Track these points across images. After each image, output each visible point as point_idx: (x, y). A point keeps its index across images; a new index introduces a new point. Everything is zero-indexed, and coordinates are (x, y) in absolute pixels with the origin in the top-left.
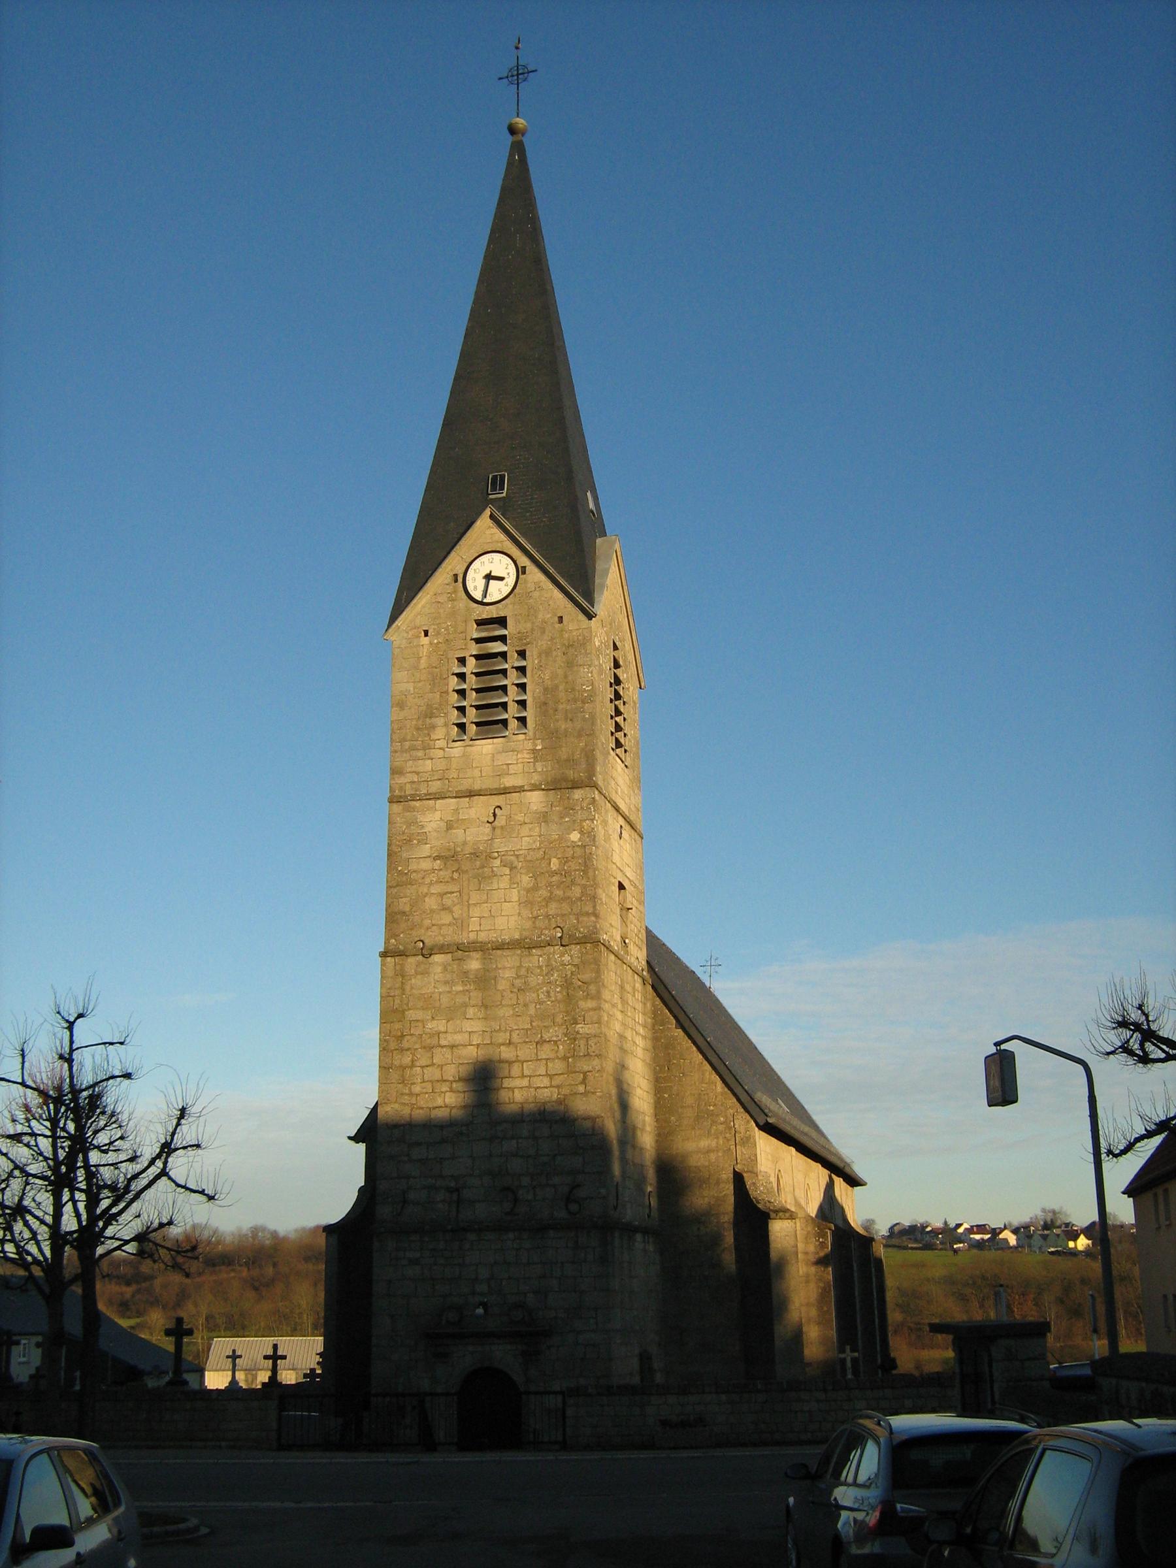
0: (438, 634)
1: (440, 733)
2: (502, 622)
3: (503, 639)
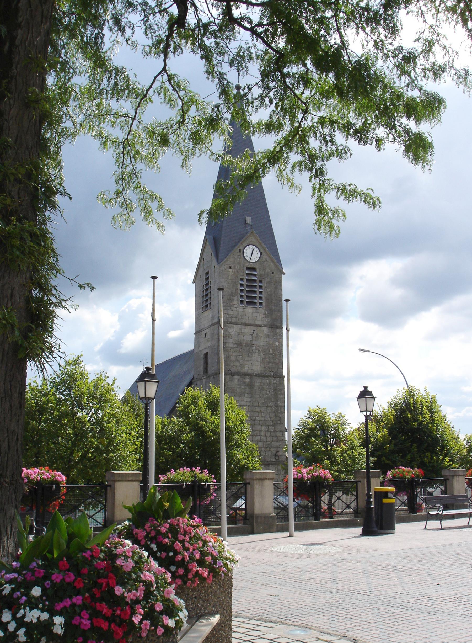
0: (235, 269)
1: (235, 302)
2: (254, 269)
3: (255, 275)
